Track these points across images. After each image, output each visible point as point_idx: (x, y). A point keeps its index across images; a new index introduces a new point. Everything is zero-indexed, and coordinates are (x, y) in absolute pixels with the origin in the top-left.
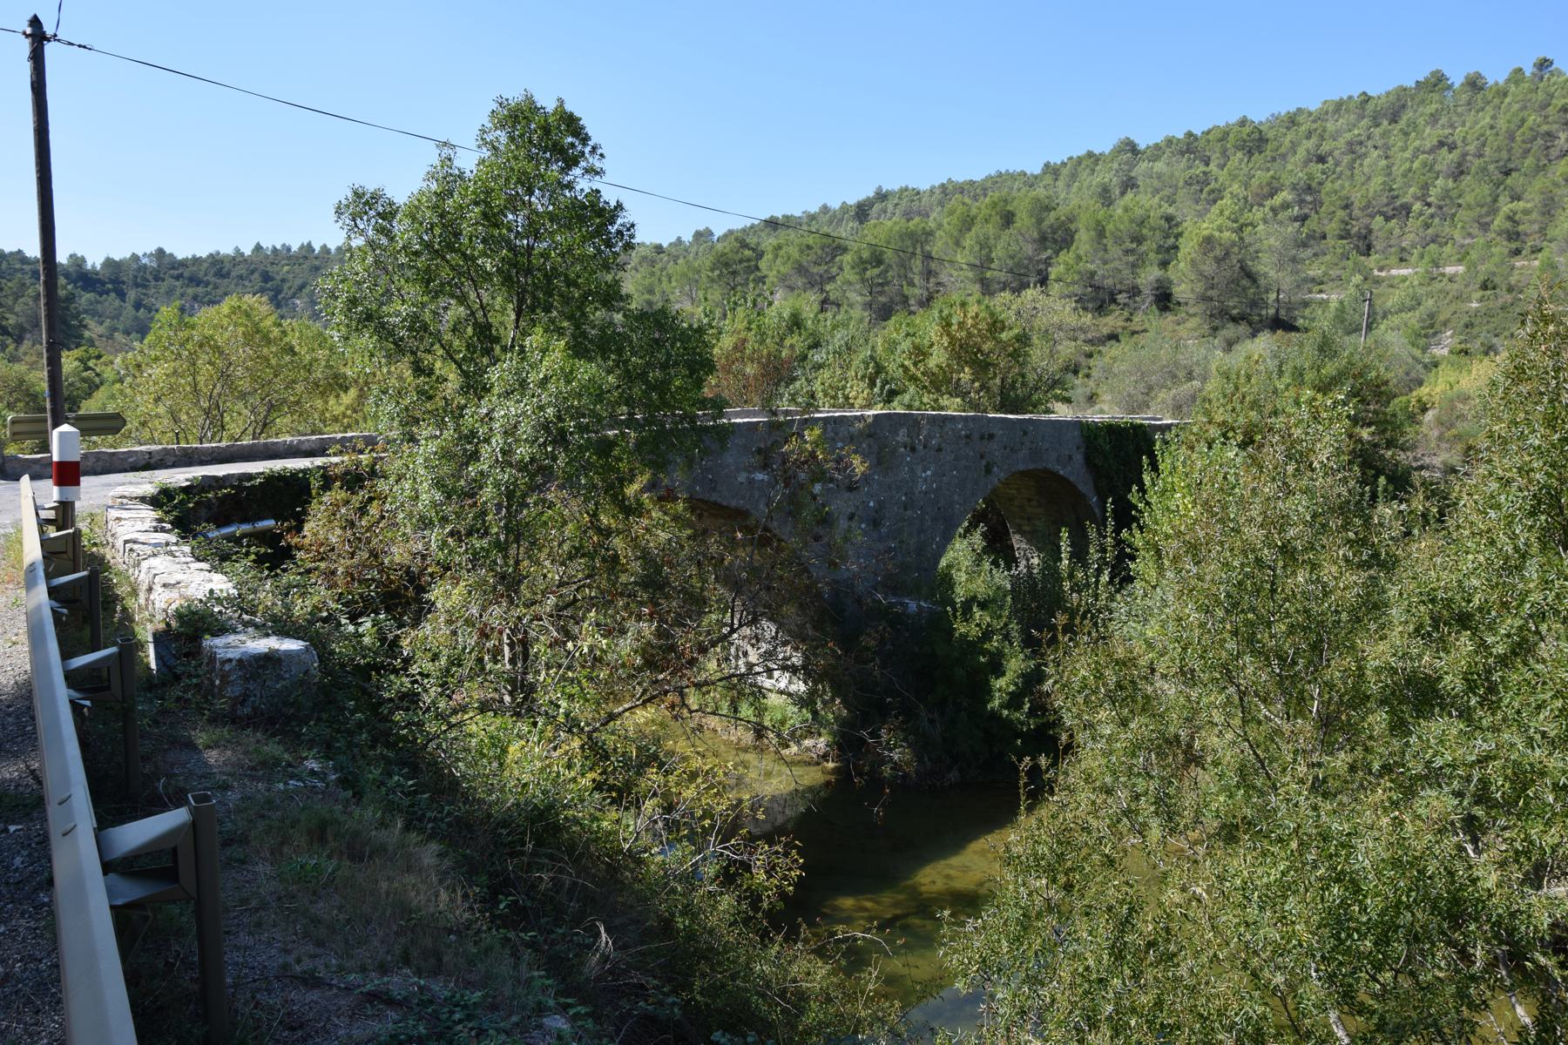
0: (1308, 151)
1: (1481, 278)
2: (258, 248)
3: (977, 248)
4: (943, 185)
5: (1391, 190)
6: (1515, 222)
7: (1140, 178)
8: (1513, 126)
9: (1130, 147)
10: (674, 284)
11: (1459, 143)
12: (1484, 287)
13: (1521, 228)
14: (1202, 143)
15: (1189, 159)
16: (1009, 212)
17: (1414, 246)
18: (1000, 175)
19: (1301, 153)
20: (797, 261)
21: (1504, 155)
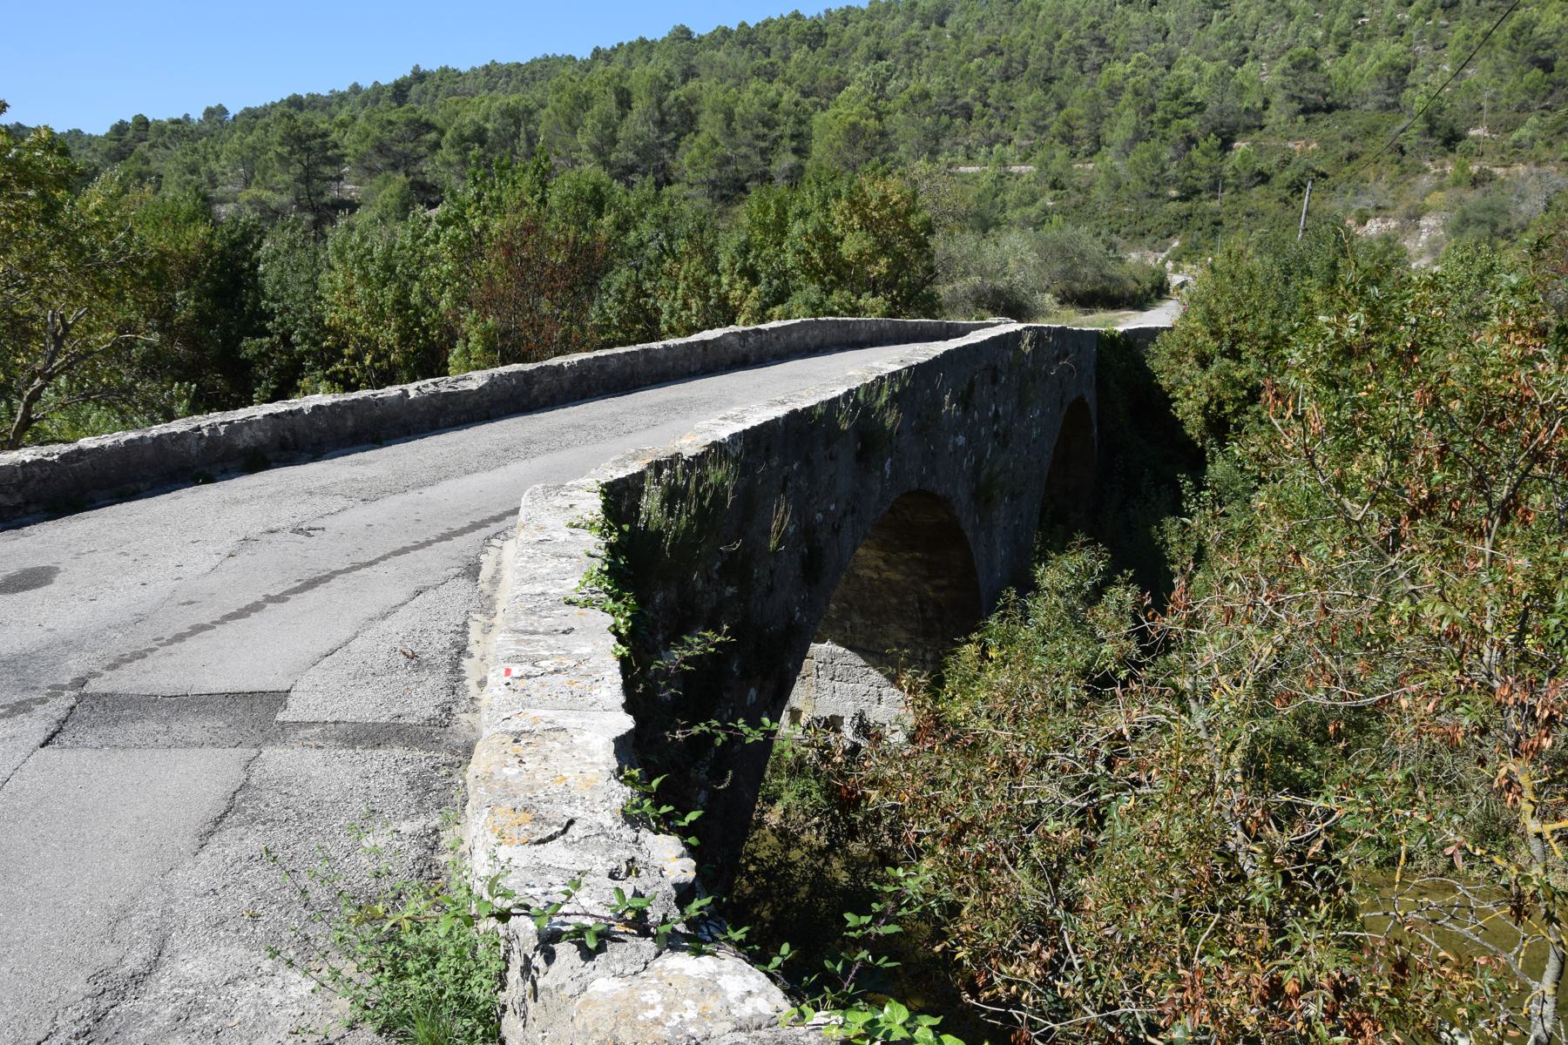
0: (868, 46)
2: (743, 25)
3: (600, 126)
4: (487, 66)
6: (1070, 126)
7: (701, 67)
8: (1050, 39)
9: (683, 34)
10: (224, 163)
11: (1005, 50)
12: (1054, 186)
13: (1076, 133)
14: (761, 36)
15: (751, 50)
17: (980, 145)
18: (547, 58)
19: (862, 50)
21: (1045, 63)
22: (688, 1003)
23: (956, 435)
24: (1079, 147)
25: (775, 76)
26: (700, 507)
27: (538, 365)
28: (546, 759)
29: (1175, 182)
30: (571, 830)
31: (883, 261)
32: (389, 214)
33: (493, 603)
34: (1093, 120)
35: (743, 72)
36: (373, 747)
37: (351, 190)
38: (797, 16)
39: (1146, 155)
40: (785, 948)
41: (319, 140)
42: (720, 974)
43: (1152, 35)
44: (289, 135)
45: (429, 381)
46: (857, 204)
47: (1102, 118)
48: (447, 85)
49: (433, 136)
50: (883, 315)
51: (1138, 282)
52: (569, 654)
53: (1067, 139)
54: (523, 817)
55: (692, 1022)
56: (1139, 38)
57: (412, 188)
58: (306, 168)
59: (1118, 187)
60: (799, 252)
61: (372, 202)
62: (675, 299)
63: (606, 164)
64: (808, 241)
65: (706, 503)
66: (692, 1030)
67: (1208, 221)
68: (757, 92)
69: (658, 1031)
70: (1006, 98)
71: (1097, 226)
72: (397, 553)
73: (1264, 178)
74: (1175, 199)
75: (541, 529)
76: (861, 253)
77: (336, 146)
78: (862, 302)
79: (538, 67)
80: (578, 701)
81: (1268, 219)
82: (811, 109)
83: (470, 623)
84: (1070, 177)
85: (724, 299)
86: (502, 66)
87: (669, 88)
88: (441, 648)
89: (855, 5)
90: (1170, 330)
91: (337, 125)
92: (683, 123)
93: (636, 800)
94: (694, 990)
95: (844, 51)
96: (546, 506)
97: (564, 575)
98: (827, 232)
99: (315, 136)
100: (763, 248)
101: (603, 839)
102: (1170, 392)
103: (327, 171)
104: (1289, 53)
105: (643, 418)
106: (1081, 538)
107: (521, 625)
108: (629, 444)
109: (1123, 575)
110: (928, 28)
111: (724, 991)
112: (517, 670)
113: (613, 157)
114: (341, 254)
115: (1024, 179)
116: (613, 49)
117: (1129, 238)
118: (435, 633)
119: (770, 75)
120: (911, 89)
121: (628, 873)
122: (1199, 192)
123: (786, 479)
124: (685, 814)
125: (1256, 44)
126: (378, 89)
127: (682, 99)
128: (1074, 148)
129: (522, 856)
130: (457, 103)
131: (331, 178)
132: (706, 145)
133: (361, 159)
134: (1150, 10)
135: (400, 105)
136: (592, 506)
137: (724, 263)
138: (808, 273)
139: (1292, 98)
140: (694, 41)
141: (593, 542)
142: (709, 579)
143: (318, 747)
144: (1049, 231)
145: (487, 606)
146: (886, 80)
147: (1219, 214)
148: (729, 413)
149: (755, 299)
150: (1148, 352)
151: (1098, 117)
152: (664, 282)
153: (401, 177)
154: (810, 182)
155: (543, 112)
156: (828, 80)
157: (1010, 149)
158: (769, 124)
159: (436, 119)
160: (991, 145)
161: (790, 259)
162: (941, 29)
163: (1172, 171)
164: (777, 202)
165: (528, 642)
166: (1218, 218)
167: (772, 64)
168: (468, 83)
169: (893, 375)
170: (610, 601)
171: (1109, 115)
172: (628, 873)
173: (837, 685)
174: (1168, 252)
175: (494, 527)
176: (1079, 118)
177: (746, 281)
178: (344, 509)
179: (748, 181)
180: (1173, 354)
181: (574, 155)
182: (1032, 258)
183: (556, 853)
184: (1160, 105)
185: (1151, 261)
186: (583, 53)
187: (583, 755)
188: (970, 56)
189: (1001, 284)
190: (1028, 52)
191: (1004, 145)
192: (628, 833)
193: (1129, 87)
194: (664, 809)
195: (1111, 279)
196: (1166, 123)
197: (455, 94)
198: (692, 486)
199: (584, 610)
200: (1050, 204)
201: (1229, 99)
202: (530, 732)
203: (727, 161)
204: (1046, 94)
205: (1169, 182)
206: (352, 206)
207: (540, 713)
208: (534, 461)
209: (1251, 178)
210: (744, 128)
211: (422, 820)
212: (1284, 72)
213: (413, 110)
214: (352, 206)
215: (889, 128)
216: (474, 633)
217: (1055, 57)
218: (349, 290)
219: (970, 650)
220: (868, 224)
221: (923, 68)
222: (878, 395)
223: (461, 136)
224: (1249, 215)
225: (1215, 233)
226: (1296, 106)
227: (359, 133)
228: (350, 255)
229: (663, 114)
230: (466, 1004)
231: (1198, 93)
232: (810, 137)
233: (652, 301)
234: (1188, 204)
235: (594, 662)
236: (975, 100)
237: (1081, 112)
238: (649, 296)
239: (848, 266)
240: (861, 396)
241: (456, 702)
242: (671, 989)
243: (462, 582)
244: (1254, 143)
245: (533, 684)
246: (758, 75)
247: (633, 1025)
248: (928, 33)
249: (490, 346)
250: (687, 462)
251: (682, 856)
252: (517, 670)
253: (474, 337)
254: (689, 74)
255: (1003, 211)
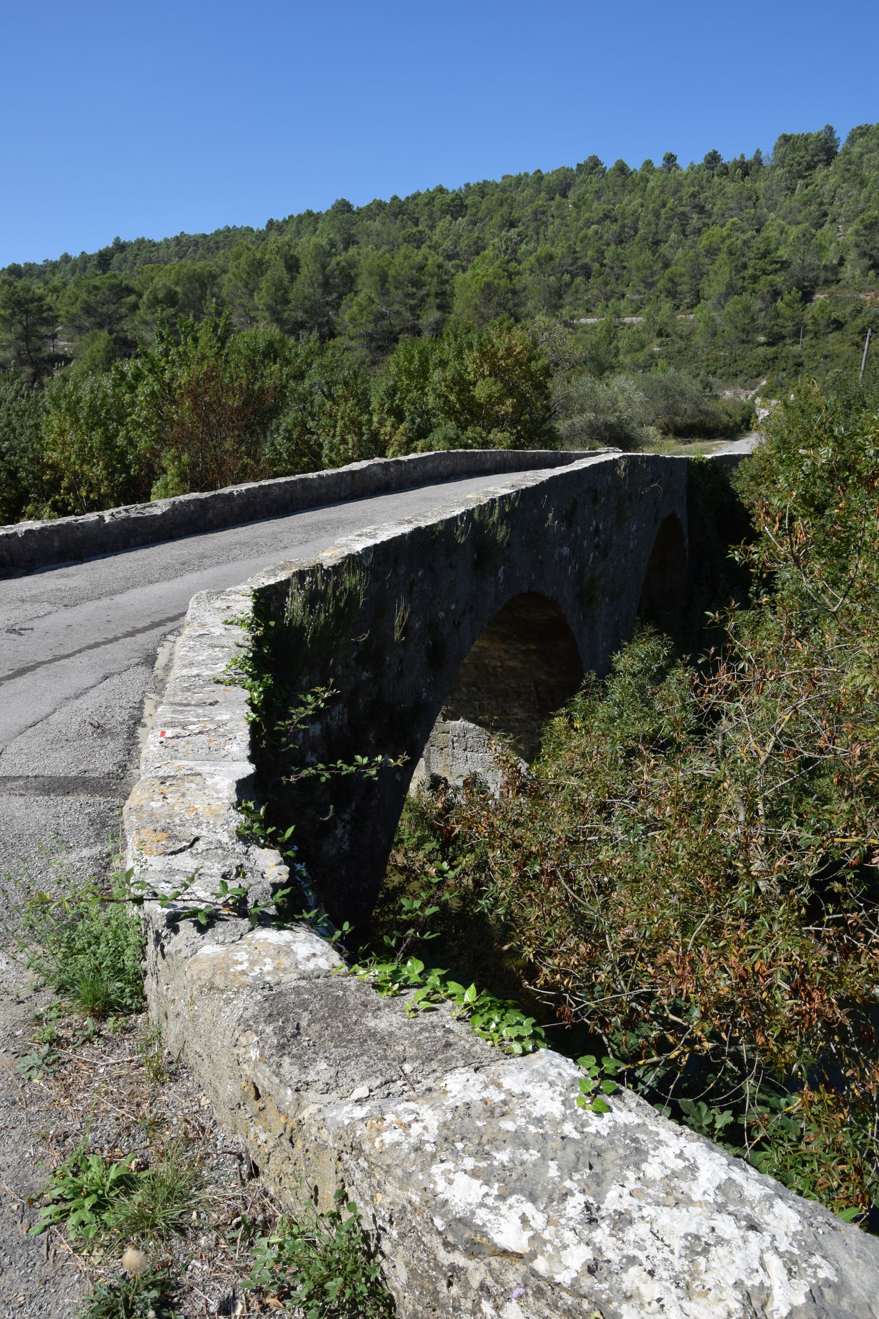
0: (502, 216)
1: (657, 327)
2: (395, 198)
4: (177, 238)
5: (575, 252)
6: (673, 282)
8: (657, 207)
9: (344, 207)
11: (619, 217)
12: (660, 334)
13: (679, 288)
14: (411, 207)
15: (402, 220)
16: (292, 257)
18: (228, 229)
19: (497, 220)
20: (85, 302)
22: (268, 960)
23: (561, 547)
24: (681, 300)
25: (423, 243)
26: (337, 607)
27: (212, 493)
28: (183, 795)
29: (763, 329)
30: (196, 845)
31: (509, 402)
32: (97, 366)
33: (164, 688)
34: (694, 277)
35: (396, 239)
36: (64, 795)
37: (64, 346)
38: (441, 190)
39: (739, 307)
40: (346, 926)
41: (36, 304)
42: (294, 942)
43: (743, 202)
44: (10, 300)
45: (121, 508)
46: (488, 356)
47: (702, 275)
48: (144, 254)
49: (132, 298)
50: (509, 447)
51: (730, 416)
52: (212, 720)
53: (672, 294)
54: (161, 835)
55: (269, 973)
56: (733, 205)
57: (115, 343)
58: (25, 328)
59: (714, 334)
60: (439, 396)
61: (81, 356)
62: (334, 436)
63: (279, 321)
64: (446, 386)
65: (342, 604)
66: (268, 978)
67: (791, 362)
68: (406, 257)
69: (244, 979)
70: (618, 258)
71: (697, 368)
72: (90, 647)
73: (838, 325)
74: (763, 345)
75: (203, 625)
76: (490, 396)
77: (50, 309)
78: (491, 436)
79: (221, 237)
80: (213, 755)
81: (842, 361)
82: (453, 271)
83: (146, 700)
84: (674, 326)
85: (375, 435)
86: (190, 237)
87: (330, 255)
88: (121, 720)
89: (490, 179)
90: (749, 456)
91: (50, 291)
92: (345, 285)
93: (248, 823)
94: (272, 952)
95: (482, 220)
96: (208, 607)
97: (216, 660)
98: (462, 377)
99: (32, 300)
100: (409, 391)
101: (220, 851)
102: (750, 509)
103: (44, 330)
104: (861, 217)
105: (298, 535)
106: (650, 629)
107: (178, 699)
108: (280, 558)
109: (682, 659)
110: (553, 199)
111: (295, 953)
112: (169, 733)
113: (286, 315)
114: (55, 401)
115: (634, 328)
116: (285, 221)
117: (724, 378)
118: (117, 709)
119: (418, 241)
120: (538, 252)
121: (238, 875)
122: (783, 338)
123: (412, 584)
124: (285, 832)
125: (833, 210)
126: (84, 257)
127: (343, 264)
128: (677, 302)
129: (157, 863)
130: (152, 270)
131: (47, 336)
132: (364, 303)
133: (72, 319)
134: (743, 179)
135: (104, 272)
136: (245, 606)
137: (375, 404)
138: (447, 413)
139: (864, 255)
140: (354, 213)
141: (242, 634)
142: (347, 666)
143: (21, 795)
144: (656, 375)
145: (159, 687)
146: (518, 243)
147: (800, 356)
148: (364, 530)
149: (403, 435)
150: (732, 476)
151: (698, 274)
152: (324, 421)
153: (104, 334)
154: (448, 335)
155: (226, 277)
156: (468, 246)
157: (623, 303)
158: (417, 284)
159: (134, 284)
160: (607, 299)
161: (431, 400)
162: (564, 200)
163: (760, 322)
164: (420, 352)
165: (182, 712)
166: (800, 360)
167: (420, 232)
168: (161, 252)
169: (502, 498)
170: (250, 680)
171: (707, 274)
172: (238, 875)
173: (469, 754)
174: (757, 390)
175: (170, 626)
176: (682, 275)
177: (393, 419)
178: (50, 613)
179: (400, 333)
180: (753, 478)
181: (253, 314)
182: (639, 396)
183: (186, 862)
184: (751, 263)
185: (742, 398)
186: (260, 225)
187: (212, 792)
188: (588, 224)
189: (612, 419)
190: (638, 219)
191: (619, 299)
192: (240, 848)
193: (724, 247)
194: (270, 830)
195: (707, 413)
196: (755, 279)
197: (151, 262)
198: (330, 591)
199: (229, 688)
200: (656, 349)
201: (809, 259)
202: (174, 777)
203: (383, 316)
204: (654, 255)
205: (757, 330)
206: (67, 360)
207: (184, 763)
208: (205, 572)
209: (828, 326)
210: (396, 288)
211: (99, 848)
212: (857, 233)
213: (115, 276)
214: (67, 360)
215: (519, 287)
216: (148, 709)
217: (661, 223)
218: (63, 432)
219: (559, 722)
220: (496, 372)
221: (549, 233)
222: (491, 515)
223: (156, 298)
224: (826, 357)
225: (797, 373)
226: (866, 262)
227: (69, 297)
228: (64, 404)
229: (327, 278)
230: (119, 972)
231: (783, 253)
232: (452, 295)
233: (315, 437)
234: (774, 349)
235: (230, 725)
236: (594, 260)
237: (683, 270)
238: (313, 433)
239: (480, 406)
240: (476, 515)
241: (130, 761)
242: (256, 952)
243: (141, 669)
244: (831, 295)
245: (181, 742)
246: (409, 242)
247: (226, 975)
248: (553, 203)
249: (183, 477)
250: (327, 571)
251: (280, 864)
252: (169, 733)
253: (172, 470)
254: (350, 241)
255: (616, 356)
